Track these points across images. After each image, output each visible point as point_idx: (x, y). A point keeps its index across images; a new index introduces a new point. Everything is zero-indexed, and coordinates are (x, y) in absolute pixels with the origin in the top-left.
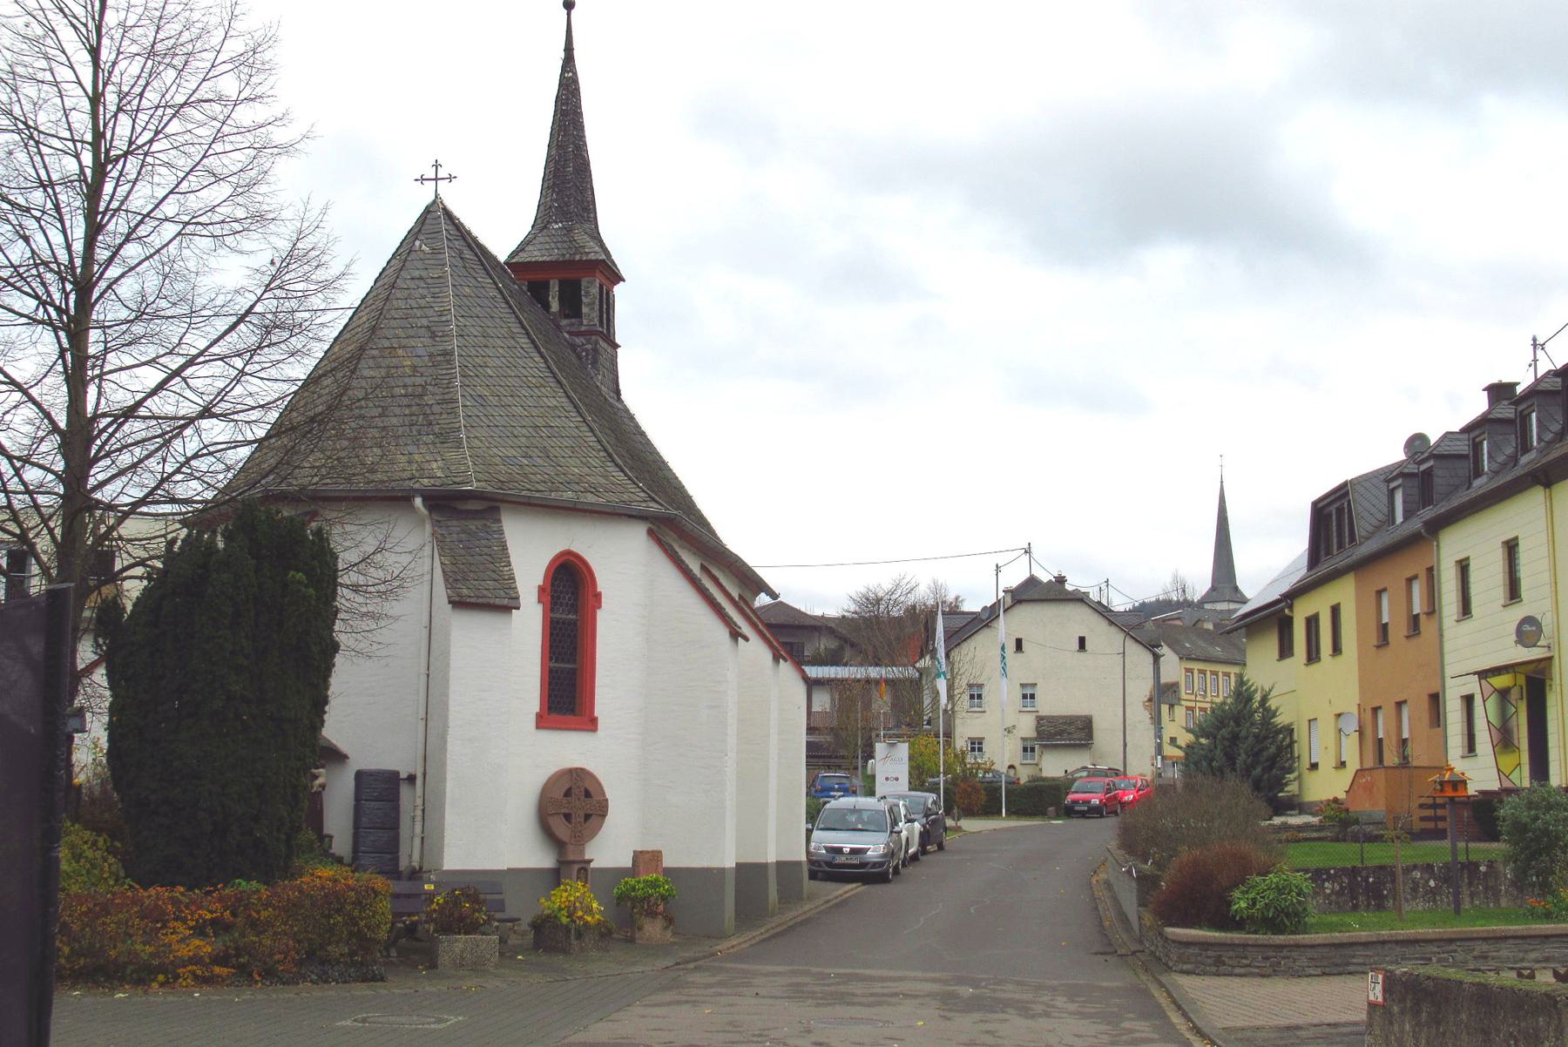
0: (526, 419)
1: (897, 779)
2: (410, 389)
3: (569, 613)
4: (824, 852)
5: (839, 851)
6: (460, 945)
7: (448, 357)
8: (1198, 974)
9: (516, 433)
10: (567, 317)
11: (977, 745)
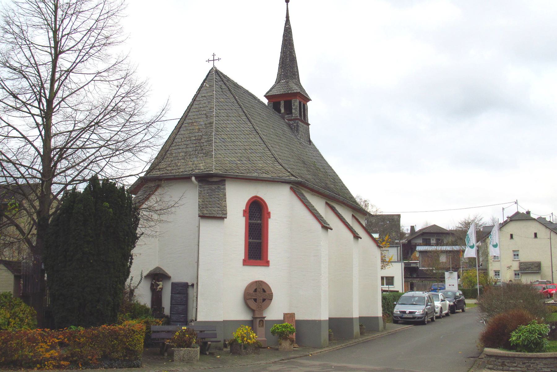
0: (242, 147)
1: (453, 285)
2: (197, 137)
3: (258, 220)
4: (399, 313)
5: (404, 312)
7: (211, 125)
8: (495, 370)
10: (288, 114)
11: (497, 273)
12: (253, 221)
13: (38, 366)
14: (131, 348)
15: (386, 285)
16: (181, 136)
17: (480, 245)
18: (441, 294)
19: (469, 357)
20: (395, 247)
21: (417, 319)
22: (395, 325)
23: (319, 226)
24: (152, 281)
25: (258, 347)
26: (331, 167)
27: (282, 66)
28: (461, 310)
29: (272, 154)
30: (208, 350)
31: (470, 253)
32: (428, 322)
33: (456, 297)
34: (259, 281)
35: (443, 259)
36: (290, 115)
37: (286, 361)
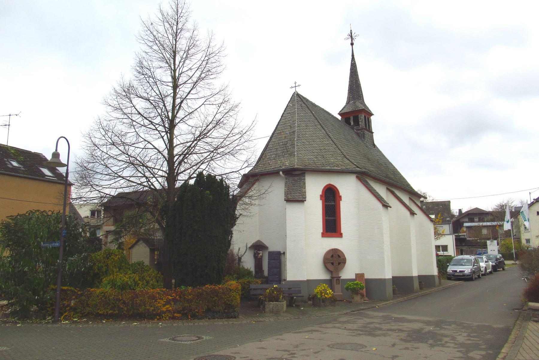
1: (494, 250)
4: (451, 272)
5: (456, 271)
6: (272, 305)
9: (313, 151)
11: (528, 241)
12: (328, 203)
13: (158, 317)
14: (229, 303)
15: (442, 251)
16: (272, 143)
17: (513, 220)
18: (485, 257)
19: (514, 309)
20: (448, 224)
21: (467, 276)
22: (449, 281)
23: (380, 205)
24: (255, 251)
25: (333, 301)
26: (391, 163)
27: (350, 91)
28: (501, 269)
29: (341, 152)
30: (294, 303)
31: (507, 226)
32: (476, 278)
33: (497, 259)
34: (334, 249)
35: (485, 232)
36: (358, 126)
37: (355, 312)
